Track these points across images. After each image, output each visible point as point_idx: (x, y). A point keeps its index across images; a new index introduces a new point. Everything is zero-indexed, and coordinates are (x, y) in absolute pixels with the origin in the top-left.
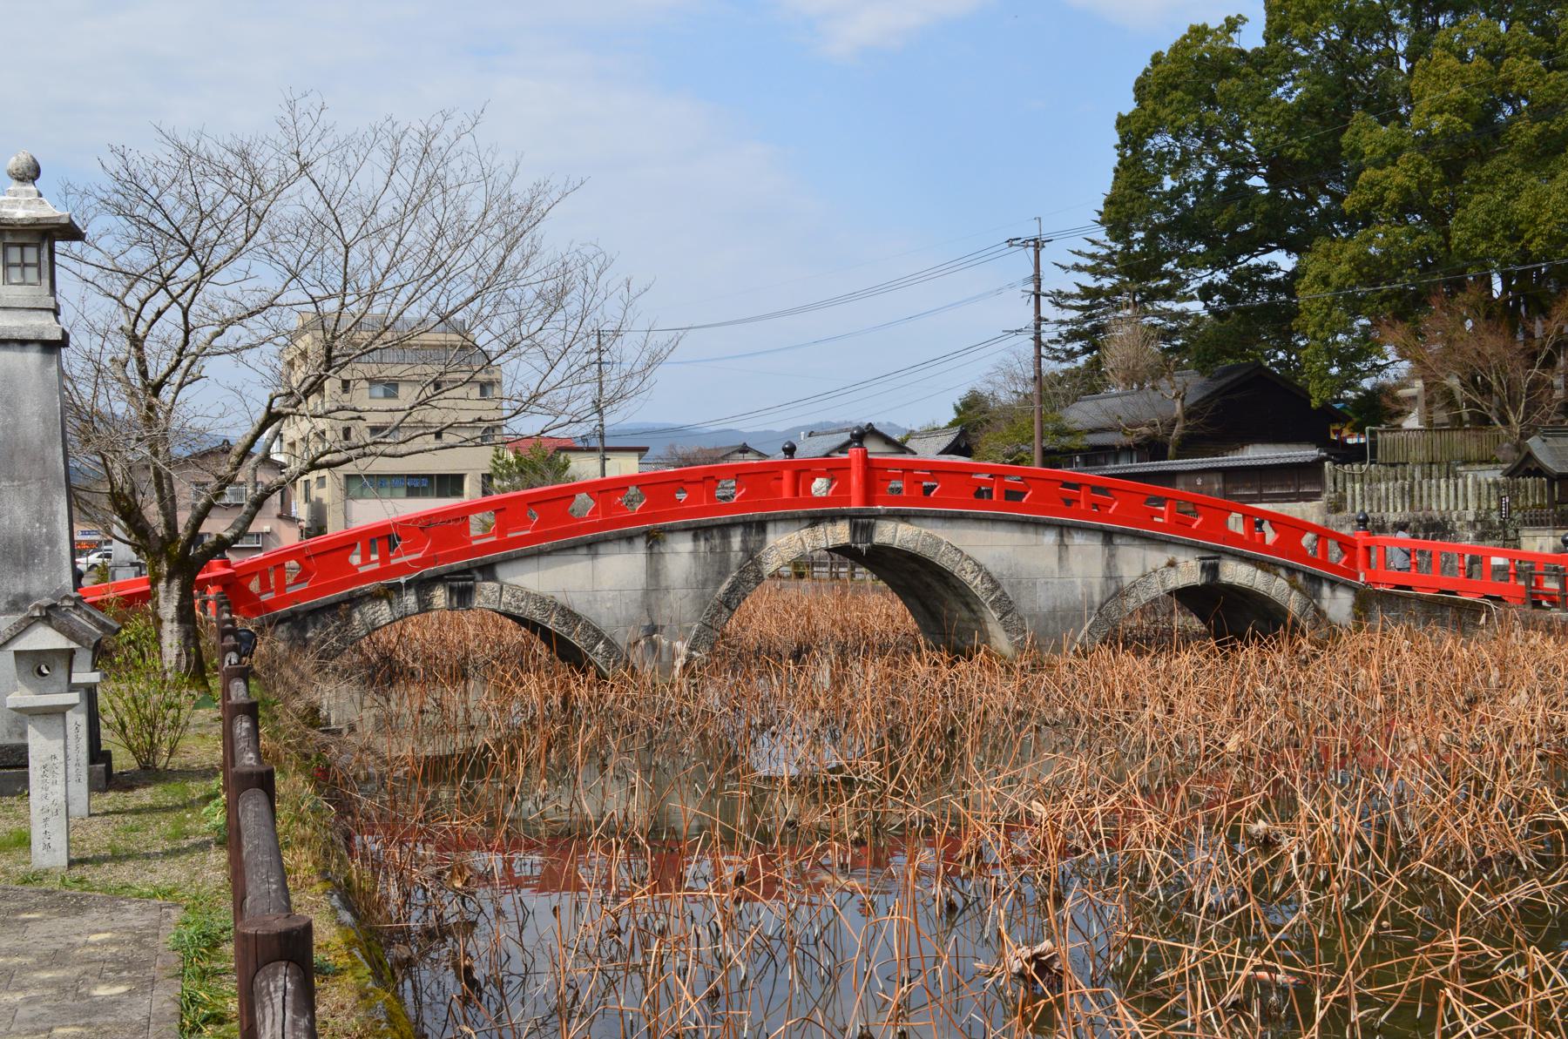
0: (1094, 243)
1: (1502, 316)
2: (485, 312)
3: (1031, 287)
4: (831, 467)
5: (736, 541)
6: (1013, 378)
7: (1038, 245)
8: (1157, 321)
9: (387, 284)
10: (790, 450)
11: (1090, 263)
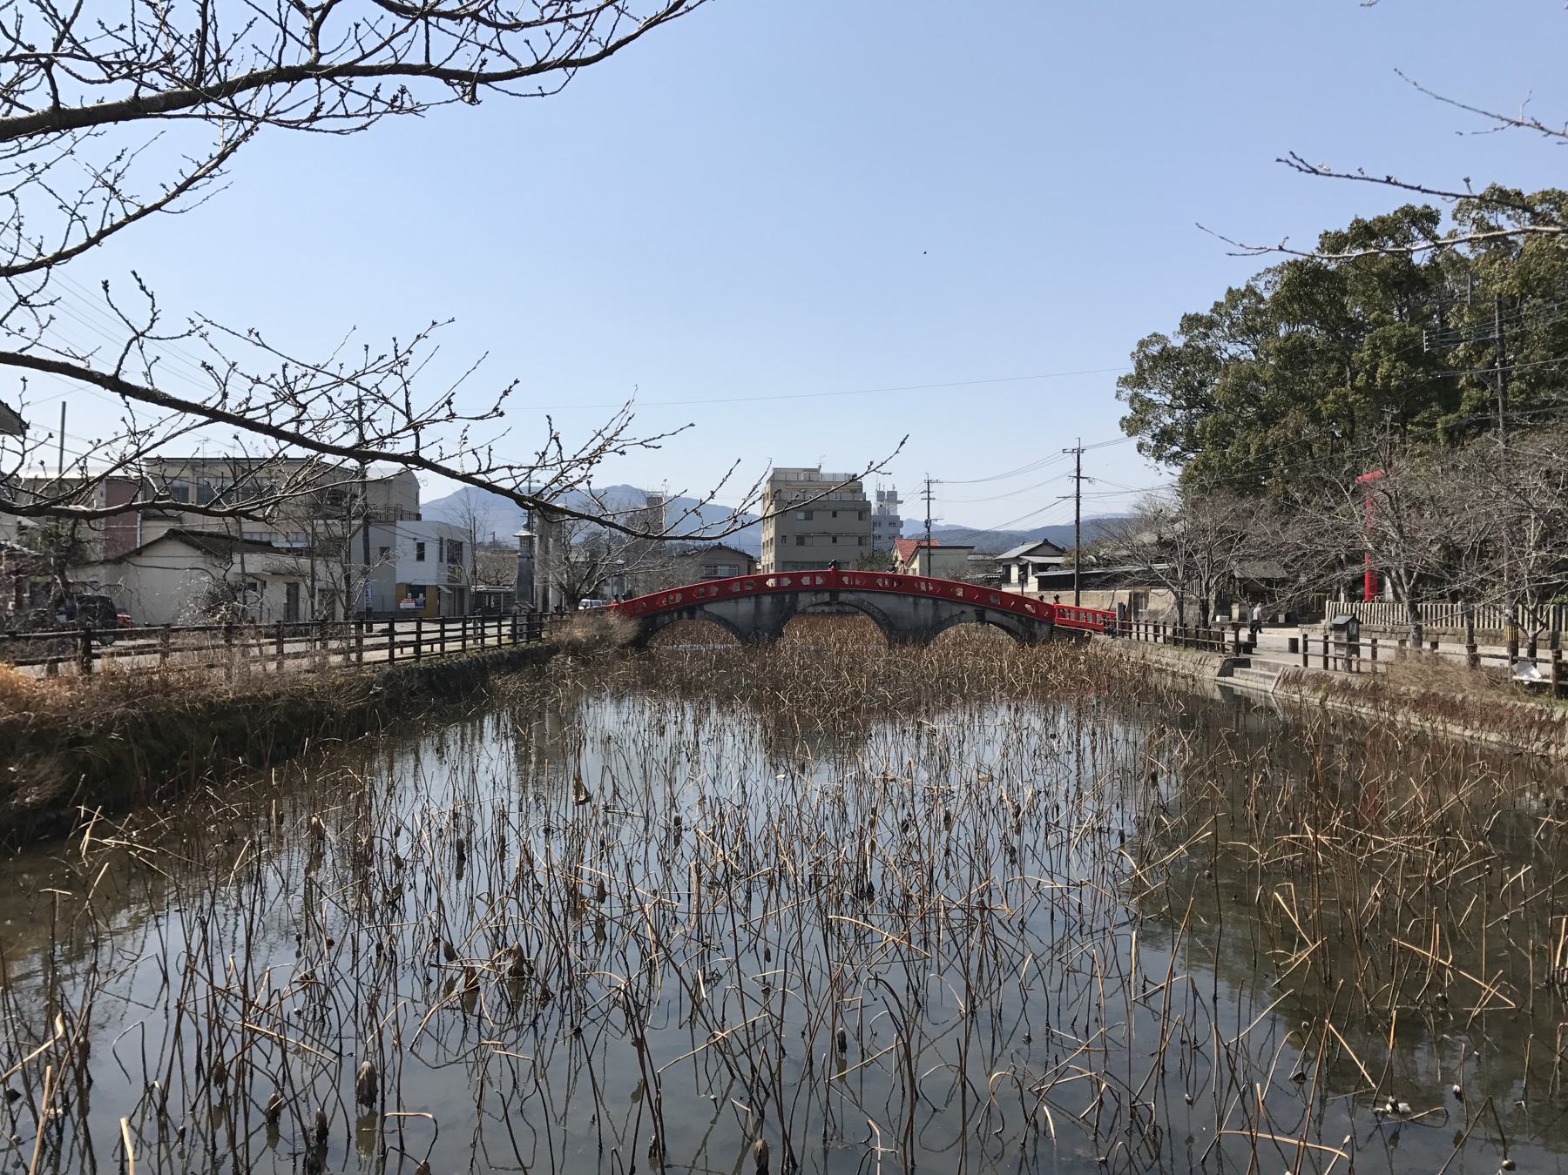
5: (787, 598)
7: (1079, 452)
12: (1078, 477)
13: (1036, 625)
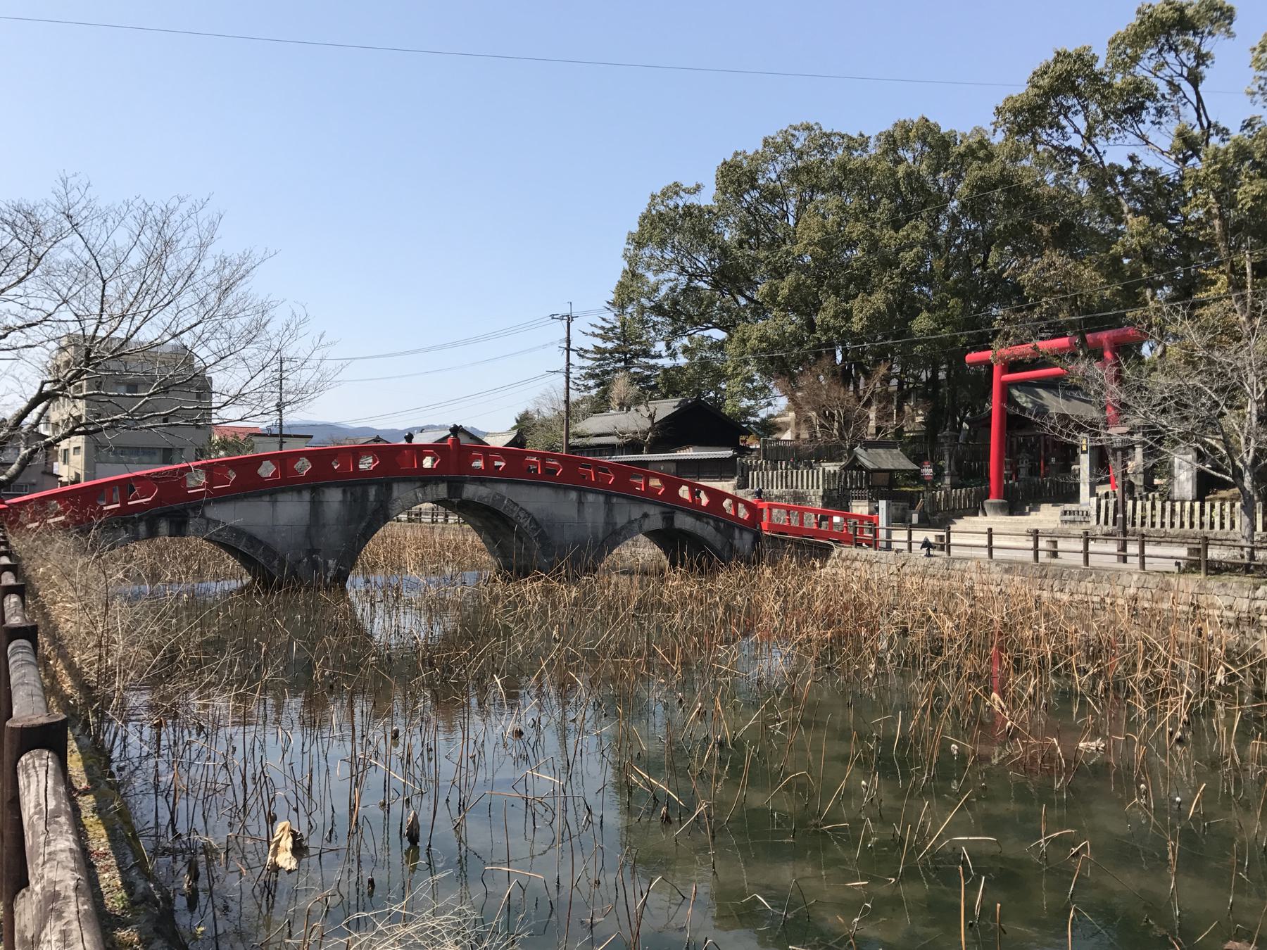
0: (604, 319)
1: (844, 377)
2: (206, 335)
3: (565, 345)
4: (437, 449)
5: (372, 492)
6: (551, 400)
7: (570, 319)
8: (639, 370)
9: (130, 312)
10: (409, 437)
11: (601, 332)
12: (568, 349)
13: (737, 532)
